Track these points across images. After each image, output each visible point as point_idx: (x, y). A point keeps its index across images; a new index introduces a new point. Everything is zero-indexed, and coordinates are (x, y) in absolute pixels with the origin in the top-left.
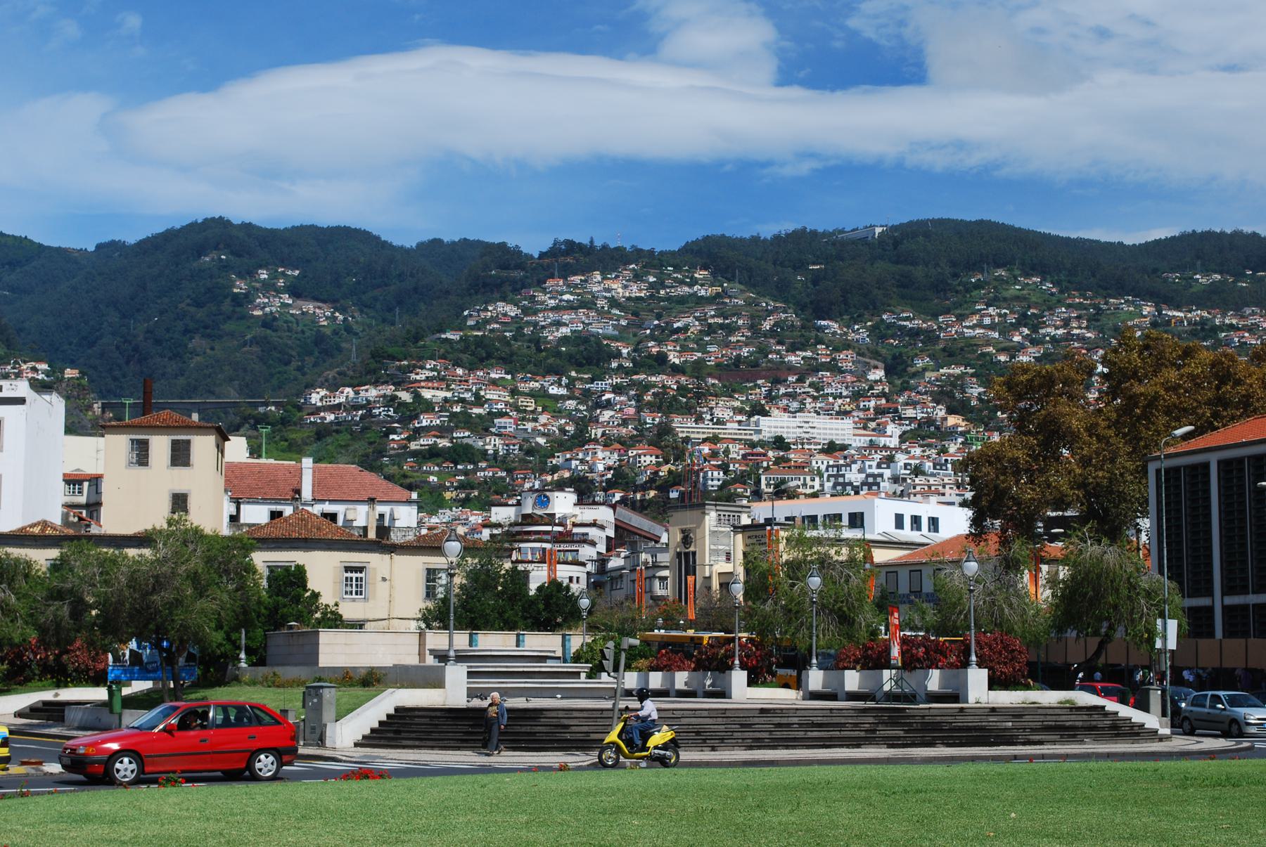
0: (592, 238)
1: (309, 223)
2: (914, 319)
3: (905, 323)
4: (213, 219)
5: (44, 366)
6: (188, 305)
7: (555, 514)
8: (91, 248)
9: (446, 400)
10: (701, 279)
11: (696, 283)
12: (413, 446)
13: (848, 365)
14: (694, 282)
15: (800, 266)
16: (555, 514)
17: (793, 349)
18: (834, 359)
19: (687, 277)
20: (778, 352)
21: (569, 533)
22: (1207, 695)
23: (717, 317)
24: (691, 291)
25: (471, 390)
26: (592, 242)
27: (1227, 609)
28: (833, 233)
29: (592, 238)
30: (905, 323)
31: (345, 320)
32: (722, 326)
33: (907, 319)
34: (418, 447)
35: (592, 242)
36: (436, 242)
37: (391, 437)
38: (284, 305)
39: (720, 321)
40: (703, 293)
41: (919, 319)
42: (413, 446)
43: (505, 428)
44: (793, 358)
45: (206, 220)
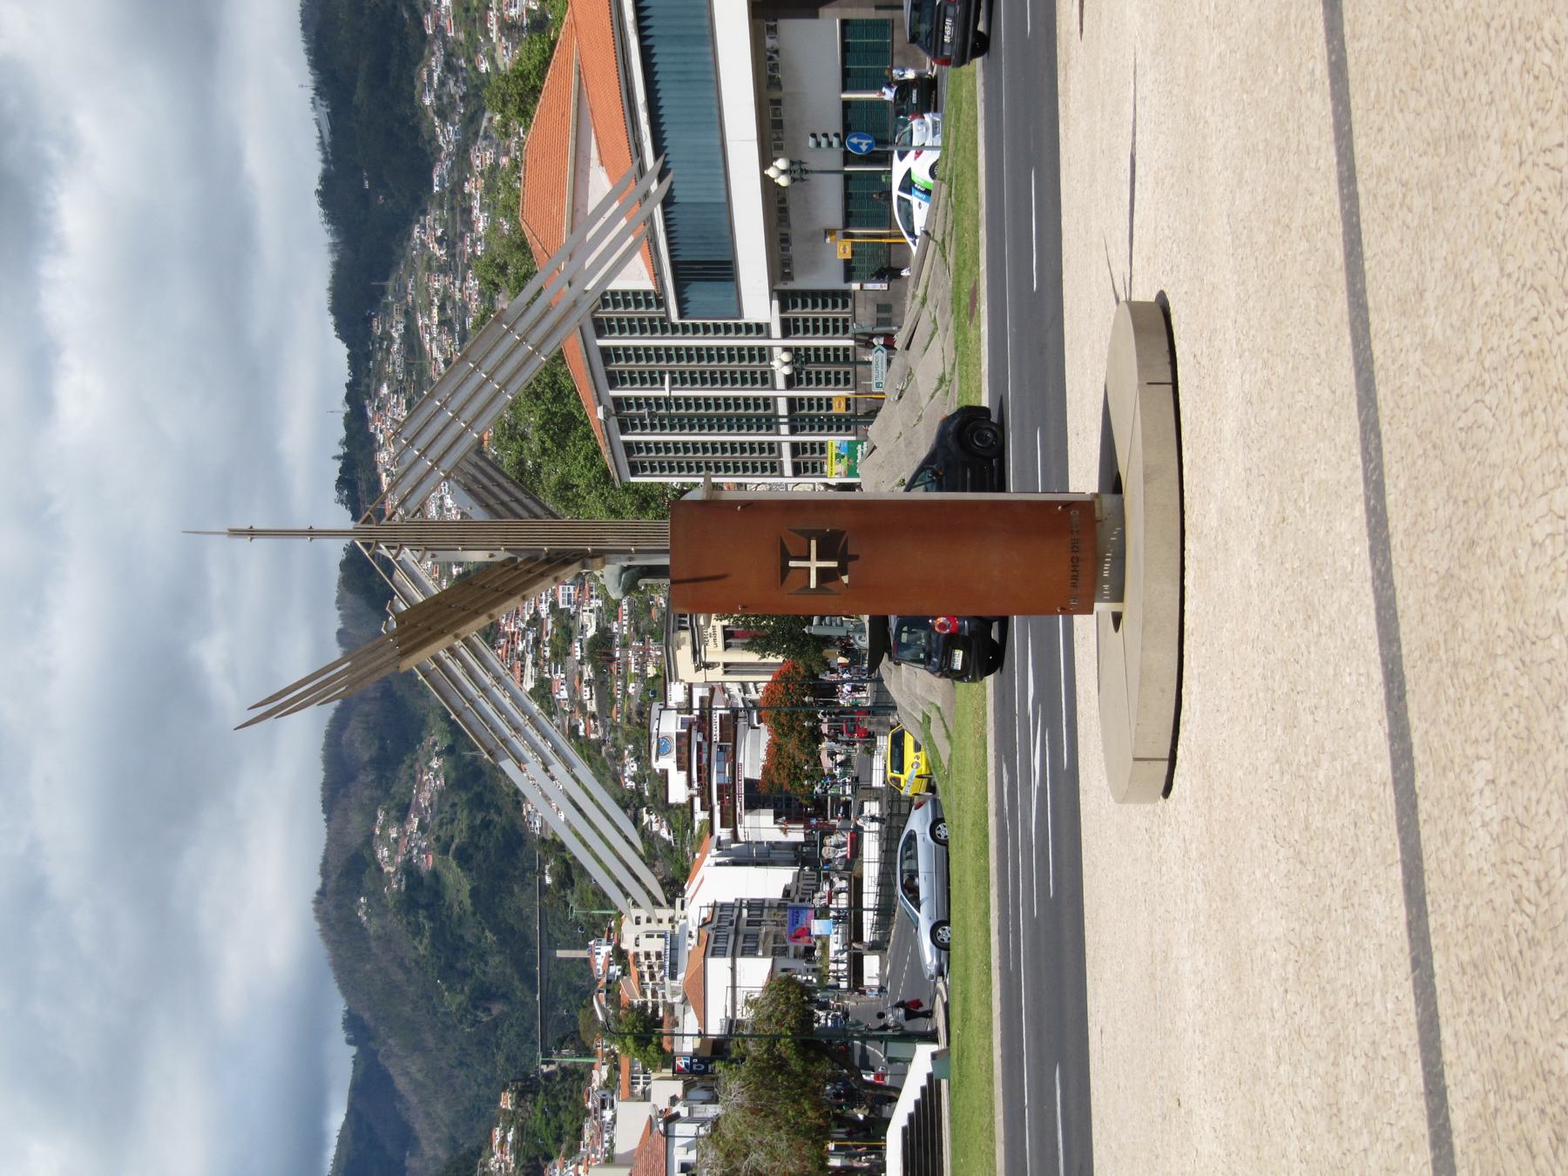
0: (334, 458)
1: (321, 766)
2: (429, 66)
3: (436, 78)
4: (316, 910)
5: (497, 1133)
6: (421, 942)
7: (677, 734)
8: (353, 1050)
9: (535, 664)
10: (383, 328)
11: (389, 333)
12: (592, 707)
13: (489, 156)
14: (386, 336)
15: (365, 198)
16: (677, 734)
17: (470, 225)
18: (482, 173)
19: (381, 344)
20: (474, 244)
21: (701, 717)
22: (899, 198)
23: (431, 311)
24: (398, 341)
25: (524, 631)
26: (338, 458)
27: (819, 558)
28: (325, 153)
29: (334, 458)
30: (436, 78)
31: (439, 754)
32: (442, 308)
33: (430, 76)
34: (594, 702)
35: (338, 458)
36: (338, 327)
37: (582, 733)
38: (422, 827)
39: (435, 311)
40: (401, 326)
41: (429, 60)
42: (592, 707)
43: (569, 595)
44: (481, 225)
45: (317, 918)
